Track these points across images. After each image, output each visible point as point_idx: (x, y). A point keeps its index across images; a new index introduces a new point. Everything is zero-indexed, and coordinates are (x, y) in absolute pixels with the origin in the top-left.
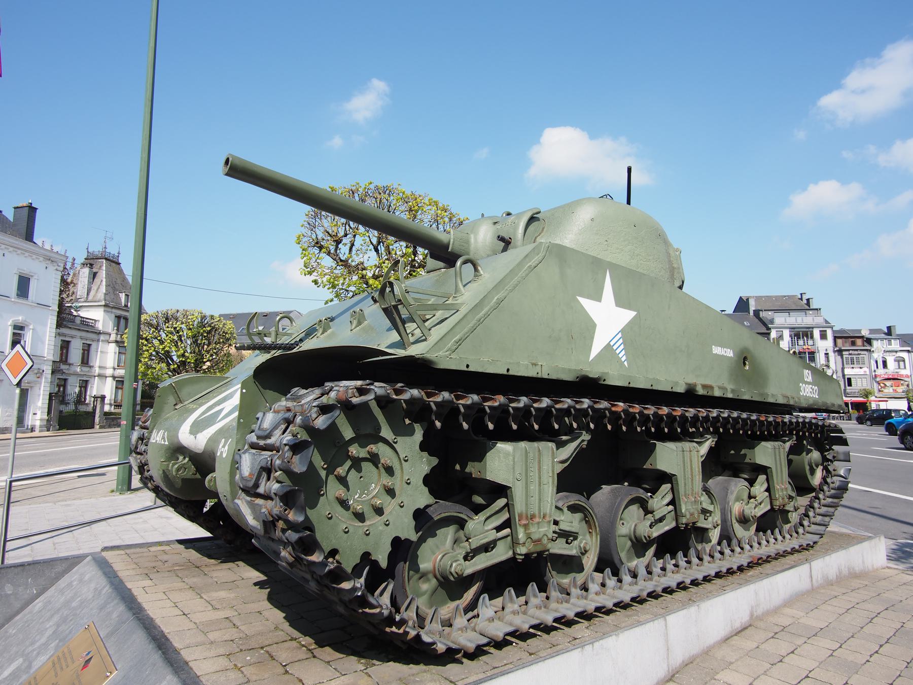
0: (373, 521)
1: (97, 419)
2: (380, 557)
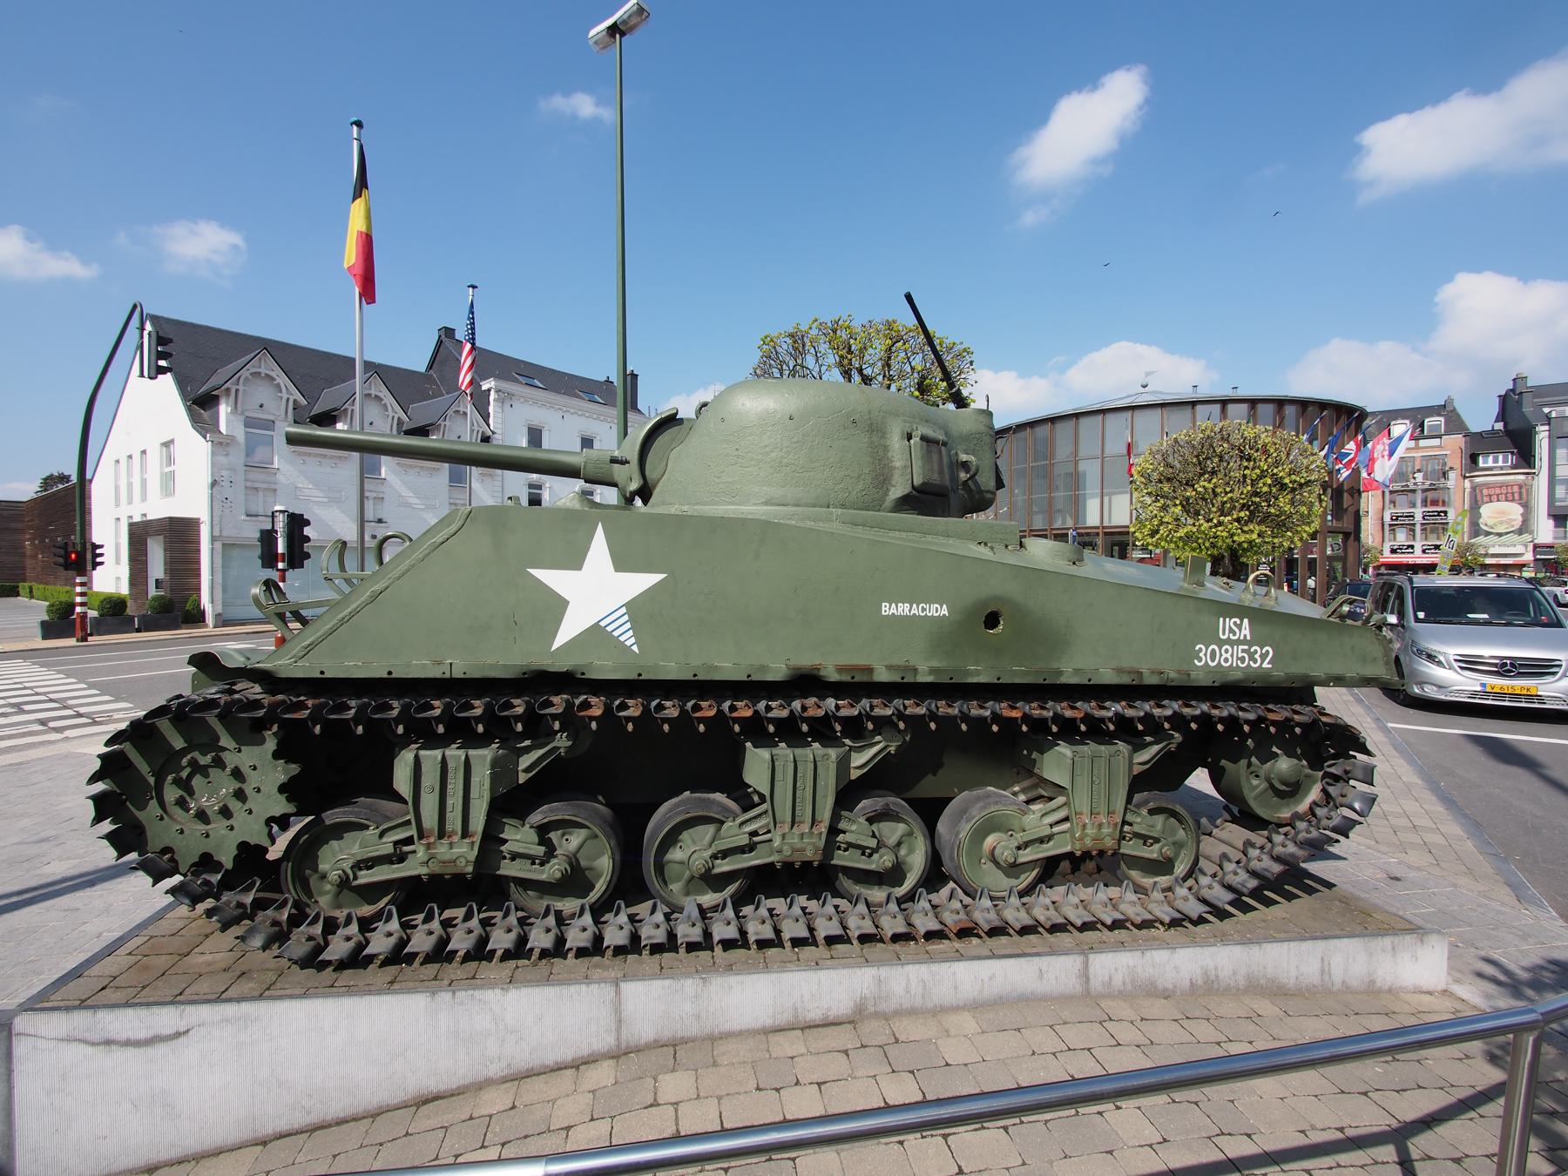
0: (218, 826)
2: (223, 858)
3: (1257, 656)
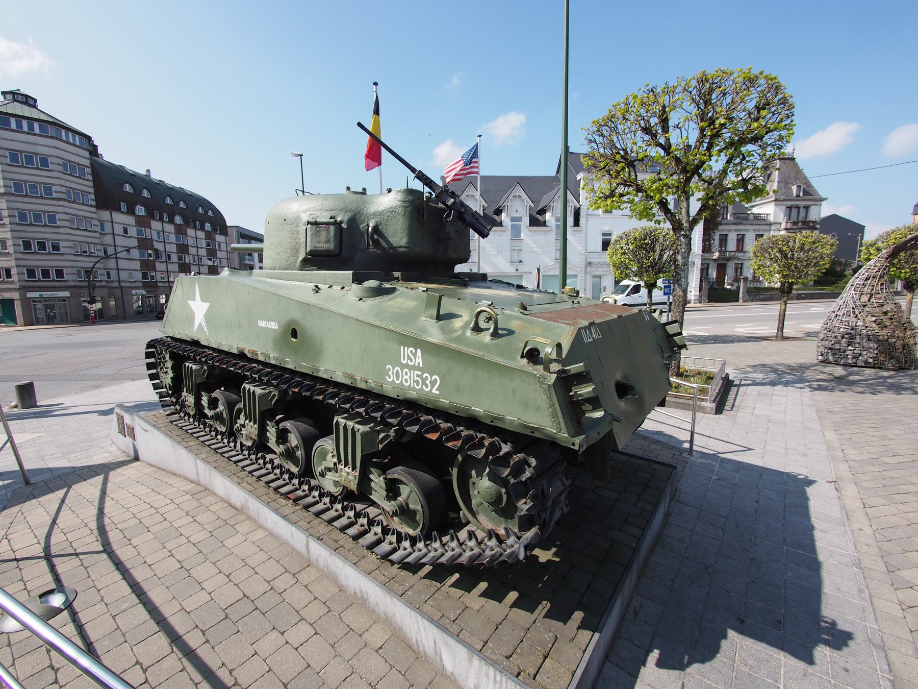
1: (741, 295)
3: (428, 382)
